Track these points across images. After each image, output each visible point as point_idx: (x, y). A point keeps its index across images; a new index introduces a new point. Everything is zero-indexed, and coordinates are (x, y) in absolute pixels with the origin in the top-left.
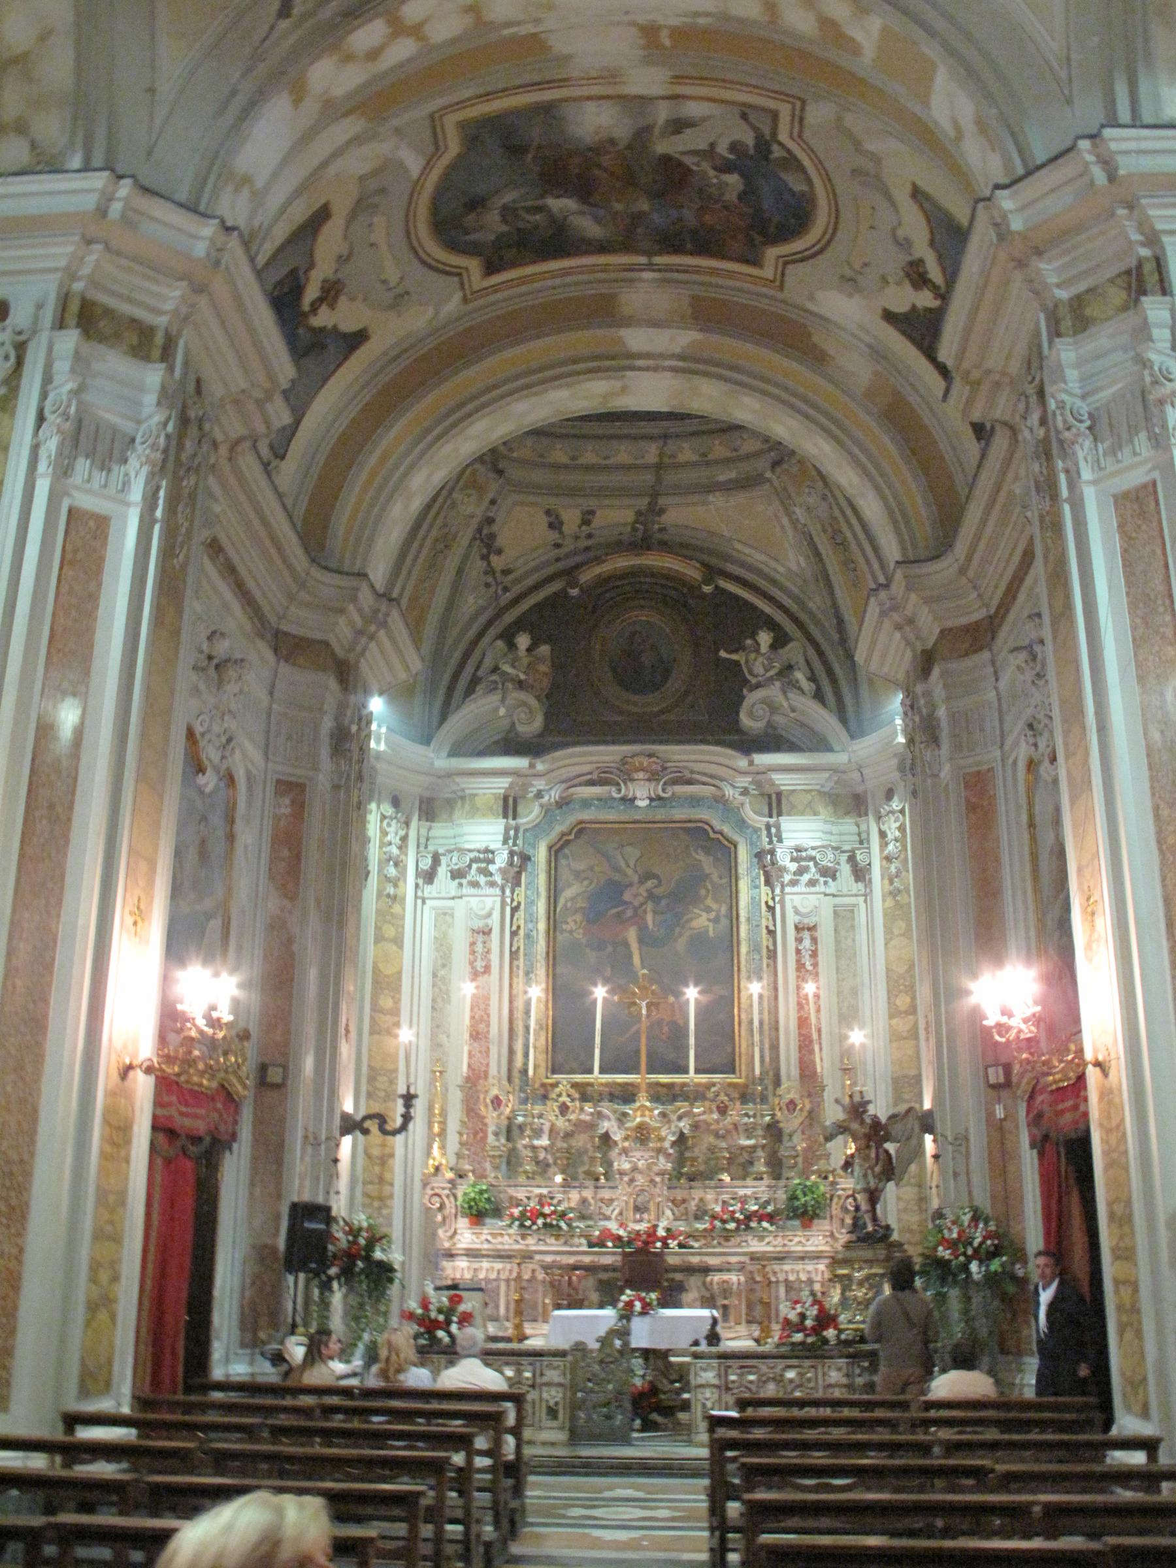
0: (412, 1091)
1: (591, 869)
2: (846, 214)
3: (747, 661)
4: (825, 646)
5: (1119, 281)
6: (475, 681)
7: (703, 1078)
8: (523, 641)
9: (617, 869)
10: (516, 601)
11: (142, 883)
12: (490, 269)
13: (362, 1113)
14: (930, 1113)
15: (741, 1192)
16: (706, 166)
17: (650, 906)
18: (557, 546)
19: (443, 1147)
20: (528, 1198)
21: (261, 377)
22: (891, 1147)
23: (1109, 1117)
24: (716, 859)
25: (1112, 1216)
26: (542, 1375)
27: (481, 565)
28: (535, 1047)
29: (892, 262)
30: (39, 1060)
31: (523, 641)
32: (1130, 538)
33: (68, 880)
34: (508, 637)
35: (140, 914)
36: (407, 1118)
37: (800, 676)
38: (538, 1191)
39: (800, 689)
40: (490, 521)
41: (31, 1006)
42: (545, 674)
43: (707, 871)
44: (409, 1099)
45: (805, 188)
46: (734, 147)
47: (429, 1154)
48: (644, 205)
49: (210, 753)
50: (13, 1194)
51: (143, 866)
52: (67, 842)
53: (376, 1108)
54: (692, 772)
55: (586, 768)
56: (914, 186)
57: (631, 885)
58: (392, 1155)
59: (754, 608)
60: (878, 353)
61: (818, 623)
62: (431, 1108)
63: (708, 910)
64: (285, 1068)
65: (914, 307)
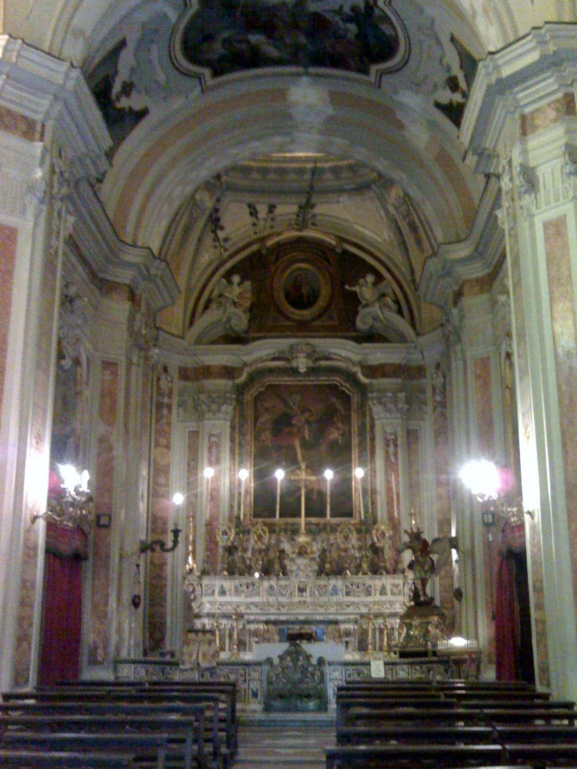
1: (274, 406)
2: (415, 50)
6: (209, 301)
10: (231, 257)
11: (40, 421)
12: (216, 74)
13: (150, 539)
14: (456, 539)
15: (356, 581)
16: (337, 18)
17: (306, 427)
19: (194, 558)
20: (241, 585)
21: (94, 147)
22: (435, 557)
25: (534, 586)
26: (249, 675)
27: (212, 236)
28: (244, 504)
29: (440, 78)
31: (236, 279)
35: (39, 438)
36: (176, 542)
37: (389, 300)
40: (216, 210)
44: (176, 532)
45: (393, 33)
46: (354, 9)
47: (186, 562)
48: (302, 39)
49: (69, 351)
51: (40, 413)
53: (156, 537)
54: (330, 353)
56: (452, 34)
59: (364, 261)
60: (432, 125)
62: (187, 537)
63: (338, 429)
64: (110, 517)
65: (451, 101)
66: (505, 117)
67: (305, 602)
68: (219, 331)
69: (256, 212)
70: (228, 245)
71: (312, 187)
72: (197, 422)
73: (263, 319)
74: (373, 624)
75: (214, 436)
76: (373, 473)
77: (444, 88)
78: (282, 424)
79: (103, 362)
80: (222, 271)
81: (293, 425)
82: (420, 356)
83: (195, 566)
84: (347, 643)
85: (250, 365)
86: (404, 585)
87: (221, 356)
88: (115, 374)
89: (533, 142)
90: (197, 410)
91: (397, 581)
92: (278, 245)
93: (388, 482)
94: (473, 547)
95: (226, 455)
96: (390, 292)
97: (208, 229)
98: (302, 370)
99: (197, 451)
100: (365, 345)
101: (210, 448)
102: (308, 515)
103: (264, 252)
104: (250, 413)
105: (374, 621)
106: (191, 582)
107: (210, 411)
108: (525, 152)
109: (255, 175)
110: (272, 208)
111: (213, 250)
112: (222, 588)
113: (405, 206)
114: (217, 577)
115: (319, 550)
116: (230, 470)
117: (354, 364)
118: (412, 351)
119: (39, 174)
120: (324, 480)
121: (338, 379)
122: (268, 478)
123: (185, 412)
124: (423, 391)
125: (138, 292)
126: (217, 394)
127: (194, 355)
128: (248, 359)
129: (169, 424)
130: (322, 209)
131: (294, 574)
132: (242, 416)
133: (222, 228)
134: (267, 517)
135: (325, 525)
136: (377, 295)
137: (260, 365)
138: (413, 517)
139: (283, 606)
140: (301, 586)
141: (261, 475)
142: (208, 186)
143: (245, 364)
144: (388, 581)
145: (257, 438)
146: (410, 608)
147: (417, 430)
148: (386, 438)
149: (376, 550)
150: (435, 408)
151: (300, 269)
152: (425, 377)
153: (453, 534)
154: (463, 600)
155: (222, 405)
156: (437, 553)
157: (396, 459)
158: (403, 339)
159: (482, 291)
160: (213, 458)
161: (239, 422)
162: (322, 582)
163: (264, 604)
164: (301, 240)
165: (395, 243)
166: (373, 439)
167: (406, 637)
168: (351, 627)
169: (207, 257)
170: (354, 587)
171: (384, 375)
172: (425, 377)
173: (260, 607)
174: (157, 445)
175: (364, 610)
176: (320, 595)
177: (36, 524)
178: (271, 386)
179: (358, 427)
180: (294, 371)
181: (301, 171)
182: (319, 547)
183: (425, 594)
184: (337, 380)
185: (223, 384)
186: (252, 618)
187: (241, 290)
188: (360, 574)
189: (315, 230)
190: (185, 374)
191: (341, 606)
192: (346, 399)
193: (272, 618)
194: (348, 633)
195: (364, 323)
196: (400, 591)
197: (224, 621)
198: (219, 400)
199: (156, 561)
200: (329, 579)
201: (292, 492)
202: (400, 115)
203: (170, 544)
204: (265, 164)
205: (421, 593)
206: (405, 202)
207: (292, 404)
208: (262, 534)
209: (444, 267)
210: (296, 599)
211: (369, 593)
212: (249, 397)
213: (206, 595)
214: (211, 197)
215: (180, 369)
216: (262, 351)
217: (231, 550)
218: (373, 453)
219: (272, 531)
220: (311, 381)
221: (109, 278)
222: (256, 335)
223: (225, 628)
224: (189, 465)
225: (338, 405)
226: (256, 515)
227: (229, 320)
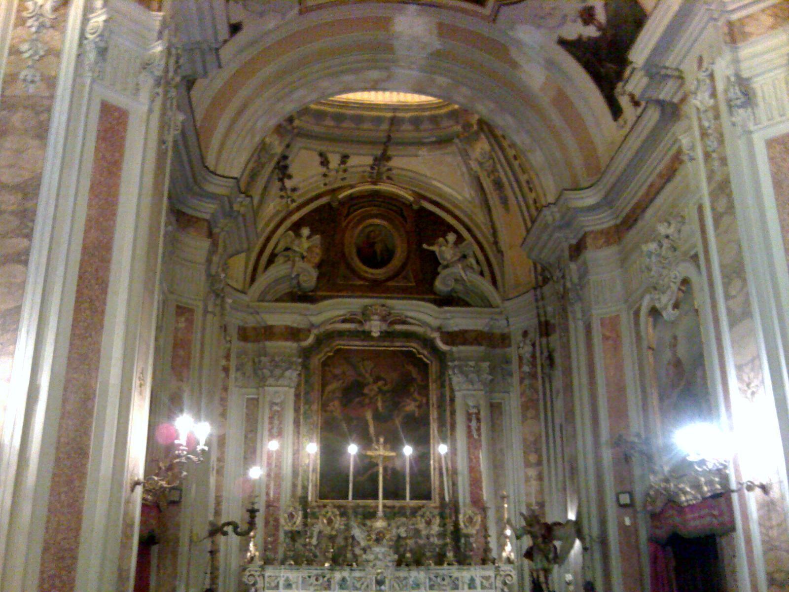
0: (256, 507)
1: (344, 373)
4: (486, 246)
5: (768, 12)
7: (414, 503)
9: (360, 375)
10: (298, 208)
15: (441, 572)
17: (379, 398)
18: (325, 175)
23: (770, 519)
27: (278, 184)
29: (574, 6)
30: (83, 476)
31: (306, 231)
32: (780, 166)
33: (103, 353)
34: (296, 227)
37: (472, 261)
38: (315, 572)
39: (472, 268)
40: (285, 157)
41: (78, 439)
42: (317, 254)
50: (64, 573)
52: (102, 327)
54: (407, 317)
55: (342, 312)
57: (369, 384)
60: (550, 64)
63: (415, 400)
66: (707, 24)
68: (284, 288)
69: (328, 162)
70: (295, 195)
71: (389, 138)
72: (257, 388)
73: (333, 277)
75: (277, 404)
76: (453, 451)
77: (575, 21)
78: (353, 392)
79: (178, 307)
80: (288, 223)
81: (364, 395)
82: (504, 322)
83: (257, 554)
85: (318, 326)
86: (496, 577)
88: (190, 322)
89: (745, 51)
90: (255, 373)
92: (351, 198)
95: (289, 427)
96: (471, 254)
97: (275, 177)
99: (256, 421)
101: (271, 418)
102: (385, 497)
103: (335, 205)
104: (316, 379)
106: (253, 573)
107: (271, 376)
108: (736, 61)
109: (330, 123)
110: (345, 158)
111: (278, 200)
112: (287, 580)
113: (491, 161)
116: (294, 444)
117: (433, 329)
118: (497, 317)
119: (158, 48)
122: (405, 442)
124: (508, 362)
125: (216, 230)
126: (281, 358)
127: (257, 313)
128: (315, 320)
130: (400, 162)
131: (371, 564)
133: (290, 177)
135: (402, 508)
136: (459, 255)
137: (329, 327)
138: (506, 500)
140: (379, 577)
141: (331, 453)
142: (279, 130)
143: (312, 325)
145: (324, 407)
147: (501, 403)
150: (522, 380)
151: (371, 225)
152: (510, 346)
155: (287, 369)
156: (559, 539)
157: (479, 435)
159: (608, 243)
160: (275, 430)
162: (402, 573)
164: (376, 194)
165: (477, 202)
166: (453, 413)
169: (273, 207)
170: (439, 580)
171: (465, 343)
177: (134, 494)
178: (339, 350)
180: (367, 335)
181: (378, 120)
184: (413, 346)
185: (290, 346)
187: (310, 244)
188: (445, 565)
189: (391, 184)
192: (424, 368)
196: (491, 585)
198: (283, 364)
200: (410, 570)
201: (367, 467)
202: (514, 53)
204: (339, 110)
206: (491, 158)
207: (363, 371)
208: (333, 518)
209: (563, 217)
212: (316, 361)
214: (281, 143)
216: (332, 311)
217: (293, 536)
219: (343, 514)
220: (387, 346)
221: (189, 212)
222: (325, 294)
224: (246, 437)
225: (414, 373)
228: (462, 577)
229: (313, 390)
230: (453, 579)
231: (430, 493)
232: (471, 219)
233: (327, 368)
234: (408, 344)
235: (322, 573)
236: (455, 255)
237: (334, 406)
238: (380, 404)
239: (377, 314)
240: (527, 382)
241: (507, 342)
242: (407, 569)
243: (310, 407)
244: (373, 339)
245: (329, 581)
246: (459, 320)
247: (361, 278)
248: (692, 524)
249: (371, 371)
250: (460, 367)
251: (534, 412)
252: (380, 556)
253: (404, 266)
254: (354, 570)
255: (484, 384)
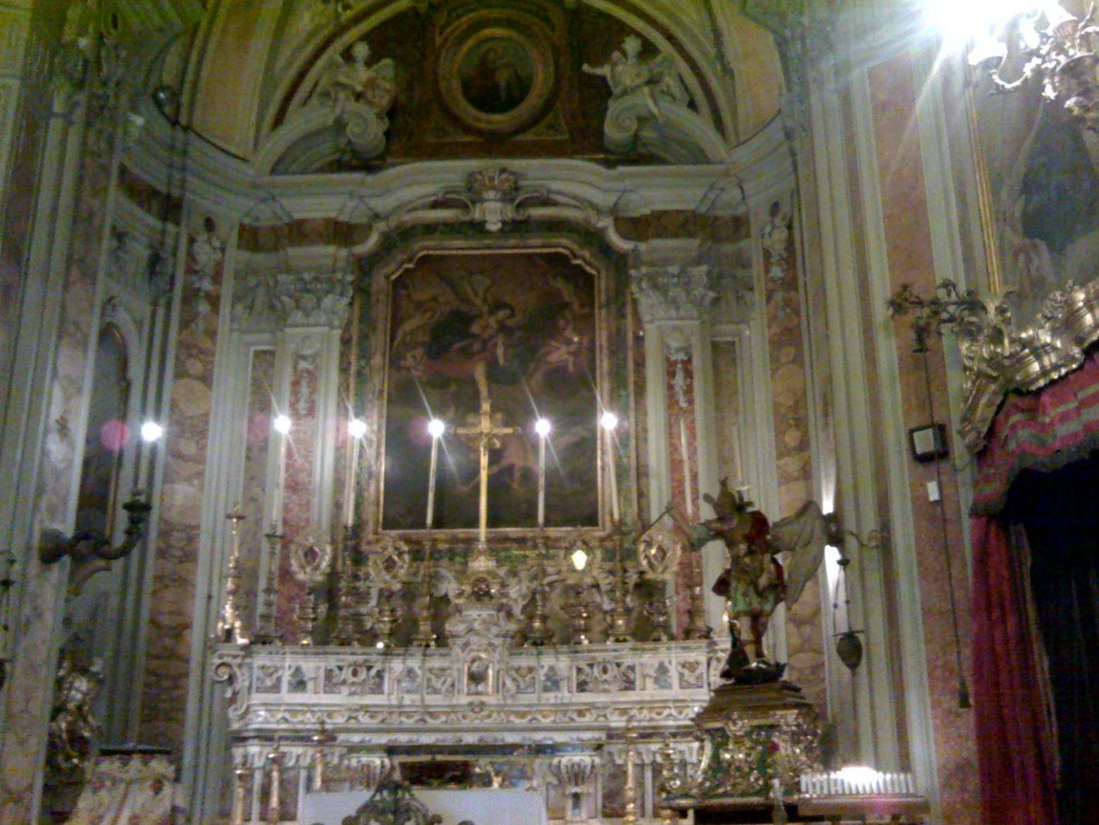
1: (435, 299)
3: (612, 76)
8: (361, 51)
9: (464, 299)
10: (357, 20)
14: (834, 518)
15: (600, 656)
17: (500, 339)
24: (576, 287)
38: (351, 658)
39: (674, 98)
42: (387, 91)
43: (567, 299)
54: (549, 191)
57: (479, 316)
58: (188, 626)
61: (694, 37)
67: (482, 705)
68: (326, 149)
72: (273, 332)
74: (639, 754)
75: (304, 358)
78: (450, 335)
80: (338, 46)
82: (736, 193)
83: (238, 624)
84: (576, 797)
85: (387, 217)
86: (709, 665)
87: (325, 200)
90: (272, 307)
91: (692, 656)
93: (673, 448)
94: (885, 527)
98: (494, 227)
100: (621, 169)
101: (296, 384)
102: (493, 521)
104: (382, 312)
105: (642, 747)
106: (226, 660)
107: (298, 307)
114: (287, 649)
115: (524, 597)
120: (530, 444)
121: (564, 241)
123: (250, 313)
124: (746, 265)
126: (313, 274)
128: (379, 204)
129: (212, 334)
131: (460, 641)
132: (366, 318)
134: (412, 526)
136: (646, 75)
137: (408, 218)
139: (432, 715)
140: (475, 667)
141: (402, 440)
143: (376, 217)
144: (672, 655)
145: (395, 362)
146: (720, 691)
147: (733, 343)
148: (668, 360)
149: (648, 590)
151: (493, 39)
152: (748, 235)
153: (828, 507)
154: (863, 669)
157: (691, 402)
158: (698, 156)
160: (302, 405)
161: (360, 330)
162: (524, 662)
163: (390, 710)
166: (640, 365)
167: (710, 767)
168: (585, 759)
170: (596, 671)
172: (748, 235)
173: (380, 717)
174: (180, 374)
175: (617, 722)
176: (519, 690)
179: (610, 338)
180: (478, 228)
182: (524, 590)
183: (759, 654)
184: (563, 244)
186: (356, 738)
190: (251, 238)
191: (565, 713)
192: (584, 283)
193: (403, 738)
194: (577, 775)
195: (621, 128)
196: (699, 677)
197: (296, 750)
199: (166, 620)
200: (539, 654)
203: (119, 540)
205: (750, 650)
210: (464, 700)
211: (629, 685)
212: (379, 281)
213: (259, 690)
215: (243, 228)
216: (412, 187)
218: (640, 390)
223: (296, 767)
225: (566, 290)
226: (389, 524)
227: (340, 125)
228: (641, 665)
229: (374, 329)
230: (623, 668)
231: (596, 512)
232: (671, 15)
233: (403, 292)
234: (555, 241)
235: (366, 661)
236: (638, 75)
237: (414, 357)
238: (500, 351)
239: (493, 188)
240: (779, 296)
241: (744, 231)
242: (534, 650)
243: (368, 364)
244: (489, 233)
245: (380, 675)
246: (653, 191)
247: (468, 130)
248: (1063, 430)
249: (486, 291)
250: (651, 278)
251: (791, 350)
252: (476, 625)
253: (549, 105)
254: (431, 655)
255: (698, 303)
